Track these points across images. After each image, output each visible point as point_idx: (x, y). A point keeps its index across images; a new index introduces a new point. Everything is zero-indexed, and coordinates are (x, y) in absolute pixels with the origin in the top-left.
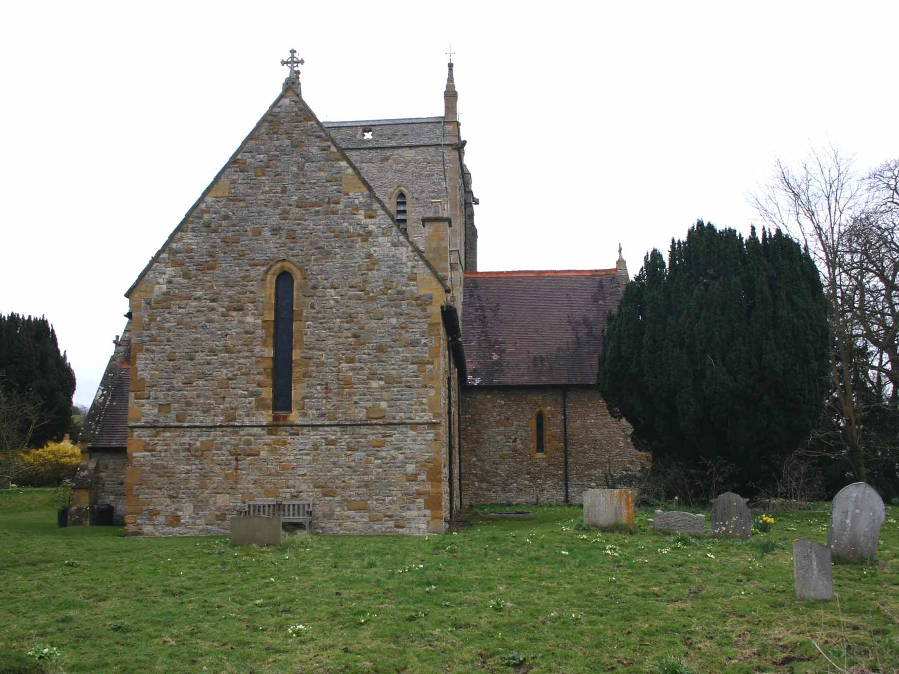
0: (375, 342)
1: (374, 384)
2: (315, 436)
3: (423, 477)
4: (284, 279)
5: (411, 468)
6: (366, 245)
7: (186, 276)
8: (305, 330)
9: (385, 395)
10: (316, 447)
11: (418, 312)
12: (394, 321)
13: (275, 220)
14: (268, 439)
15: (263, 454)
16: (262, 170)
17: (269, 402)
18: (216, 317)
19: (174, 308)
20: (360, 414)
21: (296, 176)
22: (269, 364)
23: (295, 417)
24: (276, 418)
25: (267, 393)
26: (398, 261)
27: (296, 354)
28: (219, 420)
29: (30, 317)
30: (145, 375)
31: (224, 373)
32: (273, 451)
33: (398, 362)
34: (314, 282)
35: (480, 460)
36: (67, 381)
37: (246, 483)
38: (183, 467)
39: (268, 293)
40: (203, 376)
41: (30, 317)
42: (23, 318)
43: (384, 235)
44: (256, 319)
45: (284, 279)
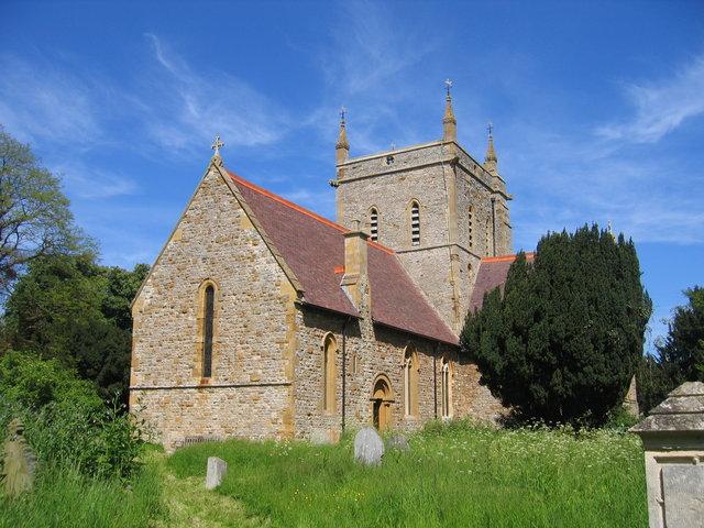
0: (256, 329)
1: (255, 358)
2: (222, 393)
3: (281, 421)
4: (210, 289)
5: (274, 415)
6: (252, 264)
7: (160, 293)
8: (219, 323)
9: (261, 365)
10: (222, 400)
11: (280, 307)
12: (266, 314)
13: (204, 253)
14: (198, 395)
15: (195, 405)
16: (198, 221)
17: (200, 371)
18: (173, 319)
19: (154, 314)
20: (246, 379)
21: (216, 222)
22: (201, 346)
23: (212, 381)
24: (203, 382)
25: (199, 366)
26: (270, 275)
27: (215, 340)
28: (174, 384)
29: (595, 228)
30: (138, 356)
31: (177, 353)
32: (200, 403)
33: (269, 344)
34: (223, 292)
35: (475, 411)
36: (638, 313)
37: (186, 425)
38: (155, 414)
39: (201, 300)
40: (167, 356)
41: (595, 228)
42: (571, 235)
43: (263, 256)
44: (195, 318)
45: (210, 289)
